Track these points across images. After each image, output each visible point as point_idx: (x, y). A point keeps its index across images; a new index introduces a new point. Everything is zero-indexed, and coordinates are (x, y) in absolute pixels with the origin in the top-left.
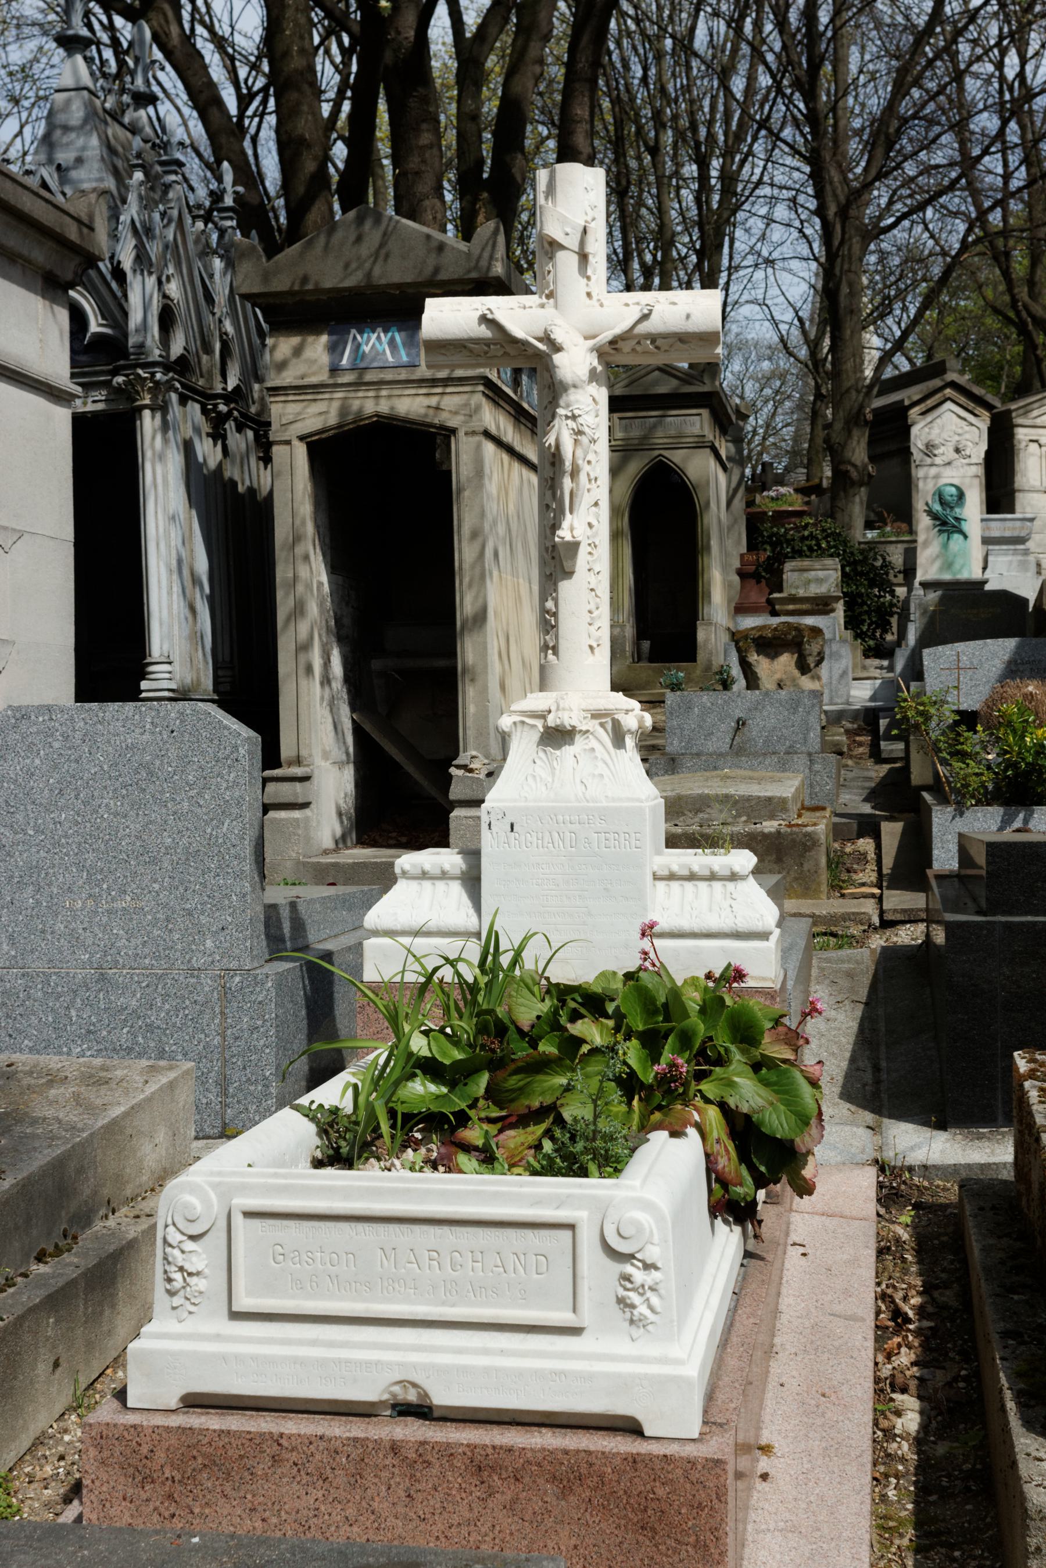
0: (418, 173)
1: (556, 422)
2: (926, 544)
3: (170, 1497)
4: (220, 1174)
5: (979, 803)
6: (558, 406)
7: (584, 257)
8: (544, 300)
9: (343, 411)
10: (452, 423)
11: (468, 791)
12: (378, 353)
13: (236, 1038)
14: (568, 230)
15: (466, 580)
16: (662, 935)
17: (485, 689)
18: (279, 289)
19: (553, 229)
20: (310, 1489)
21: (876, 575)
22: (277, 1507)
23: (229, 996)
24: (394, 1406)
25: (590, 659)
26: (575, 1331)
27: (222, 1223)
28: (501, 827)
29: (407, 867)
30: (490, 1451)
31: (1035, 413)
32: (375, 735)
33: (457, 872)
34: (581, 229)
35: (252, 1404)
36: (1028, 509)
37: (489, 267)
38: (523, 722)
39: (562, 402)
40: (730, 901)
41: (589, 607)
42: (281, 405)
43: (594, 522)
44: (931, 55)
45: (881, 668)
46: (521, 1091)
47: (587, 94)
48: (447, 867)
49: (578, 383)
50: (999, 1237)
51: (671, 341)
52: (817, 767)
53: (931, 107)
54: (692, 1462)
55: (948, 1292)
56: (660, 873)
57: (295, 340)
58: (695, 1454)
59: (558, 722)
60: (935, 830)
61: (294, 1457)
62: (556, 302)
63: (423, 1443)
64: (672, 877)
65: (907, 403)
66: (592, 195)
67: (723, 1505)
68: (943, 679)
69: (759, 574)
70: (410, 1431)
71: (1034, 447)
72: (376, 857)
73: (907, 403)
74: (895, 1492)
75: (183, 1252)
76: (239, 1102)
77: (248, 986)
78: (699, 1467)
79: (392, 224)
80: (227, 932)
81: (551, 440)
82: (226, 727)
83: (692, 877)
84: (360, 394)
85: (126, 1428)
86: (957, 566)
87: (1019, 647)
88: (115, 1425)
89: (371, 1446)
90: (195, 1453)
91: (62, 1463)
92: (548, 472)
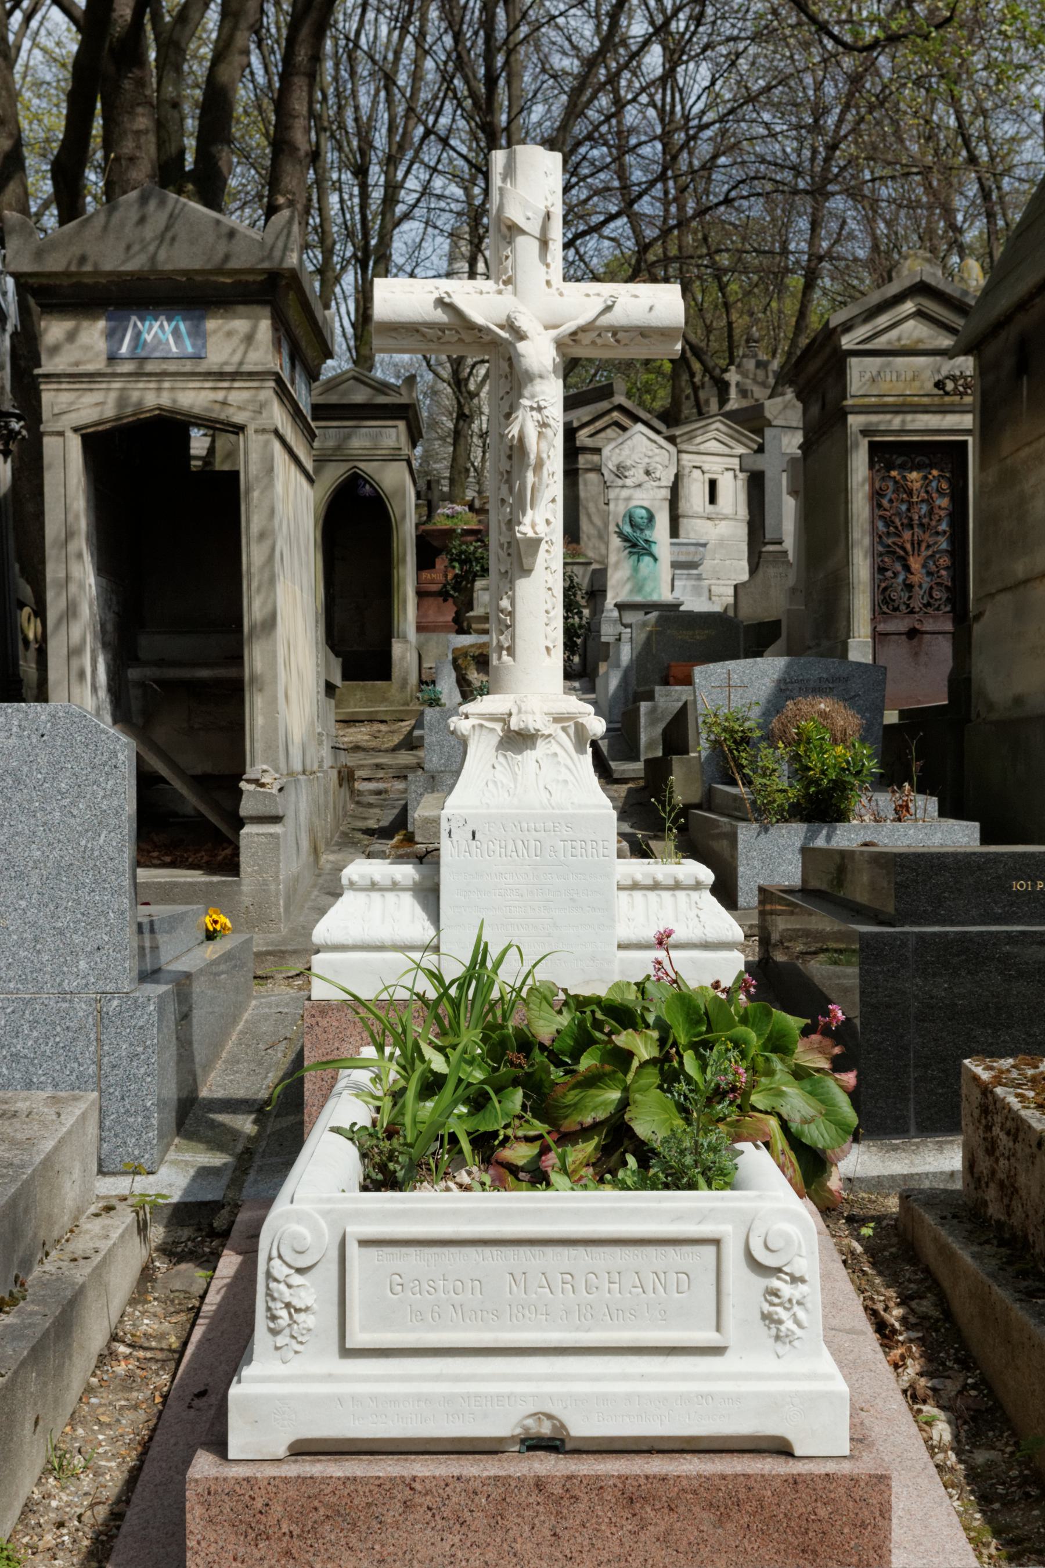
0: (132, 159)
1: (520, 413)
2: (617, 564)
3: (288, 1553)
4: (329, 1200)
6: (520, 396)
7: (544, 243)
8: (502, 286)
10: (239, 418)
12: (160, 342)
13: (114, 1067)
14: (530, 214)
15: (255, 585)
16: (678, 946)
17: (274, 700)
18: (54, 269)
19: (514, 213)
20: (446, 1535)
22: (408, 1557)
23: (106, 1021)
24: (523, 1441)
26: (717, 1351)
27: (334, 1254)
28: (461, 835)
29: (355, 878)
30: (642, 1481)
31: (699, 440)
34: (542, 214)
35: (365, 1448)
36: (692, 535)
38: (481, 726)
39: (526, 393)
41: (546, 607)
42: (53, 393)
43: (552, 519)
44: (602, 79)
46: (575, 1106)
47: (305, 88)
48: (398, 877)
50: (980, 1244)
51: (633, 334)
53: (604, 129)
54: (854, 1480)
55: (925, 1302)
56: (623, 882)
57: (68, 325)
58: (856, 1471)
59: (522, 725)
61: (428, 1500)
62: (515, 288)
63: (570, 1478)
64: (635, 886)
67: (886, 1522)
68: (714, 697)
69: (447, 592)
70: (545, 1465)
71: (697, 473)
74: (958, 1503)
75: (289, 1286)
76: (116, 1135)
77: (127, 1010)
78: (862, 1484)
79: (179, 206)
80: (103, 952)
81: (514, 431)
82: (103, 731)
83: (656, 886)
84: (141, 385)
85: (238, 1482)
86: (648, 589)
87: (789, 666)
88: (225, 1479)
89: (513, 1484)
90: (316, 1503)
91: (65, 1531)
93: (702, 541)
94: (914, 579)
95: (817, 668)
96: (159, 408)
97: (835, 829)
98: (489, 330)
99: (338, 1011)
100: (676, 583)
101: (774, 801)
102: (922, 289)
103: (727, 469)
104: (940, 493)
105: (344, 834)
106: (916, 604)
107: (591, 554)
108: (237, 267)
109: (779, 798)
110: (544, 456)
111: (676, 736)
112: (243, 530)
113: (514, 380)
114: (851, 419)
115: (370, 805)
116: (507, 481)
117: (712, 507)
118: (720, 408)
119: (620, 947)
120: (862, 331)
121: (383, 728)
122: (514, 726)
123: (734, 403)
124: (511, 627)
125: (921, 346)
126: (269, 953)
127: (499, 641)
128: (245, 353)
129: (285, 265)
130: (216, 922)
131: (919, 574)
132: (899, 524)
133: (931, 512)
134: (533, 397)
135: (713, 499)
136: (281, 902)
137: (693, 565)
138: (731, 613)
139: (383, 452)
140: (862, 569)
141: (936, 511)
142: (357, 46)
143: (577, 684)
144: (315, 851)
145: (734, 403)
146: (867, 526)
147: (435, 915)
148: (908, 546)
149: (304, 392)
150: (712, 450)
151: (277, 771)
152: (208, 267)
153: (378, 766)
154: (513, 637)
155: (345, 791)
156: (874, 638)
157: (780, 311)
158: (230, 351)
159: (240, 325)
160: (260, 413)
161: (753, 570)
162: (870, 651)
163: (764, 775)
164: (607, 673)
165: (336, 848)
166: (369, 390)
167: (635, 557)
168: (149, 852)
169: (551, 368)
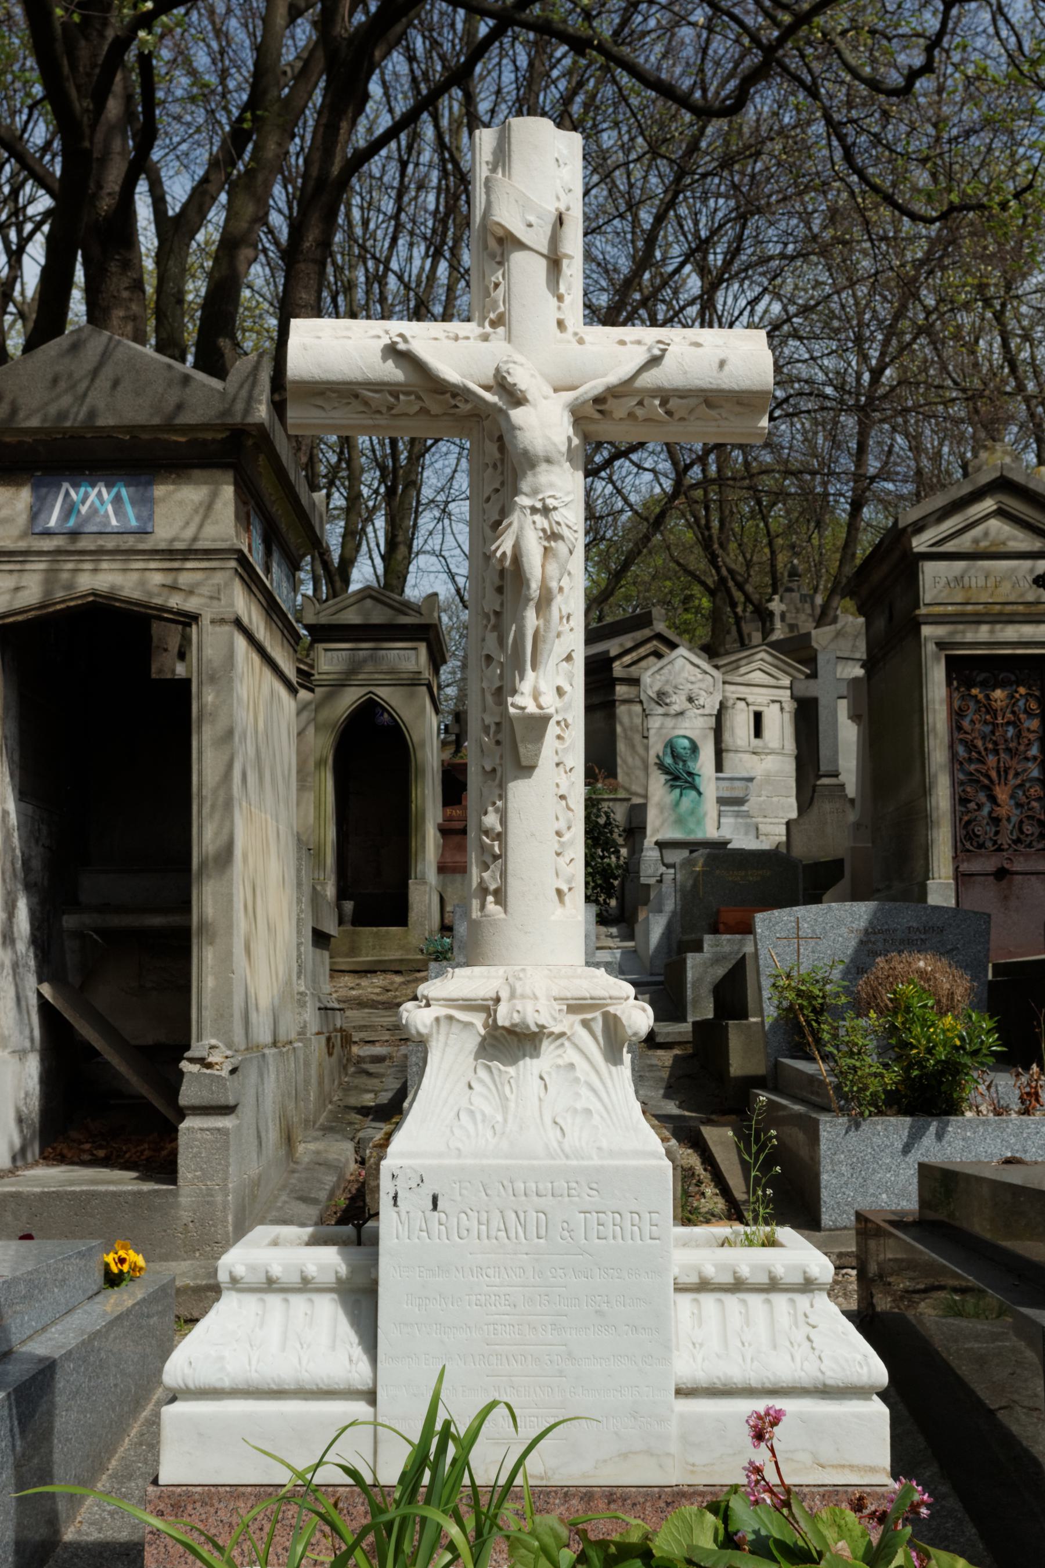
1: (515, 518)
5: (880, 1113)
6: (516, 491)
7: (555, 263)
8: (488, 329)
10: (191, 605)
11: (205, 1093)
14: (532, 219)
15: (206, 810)
17: (227, 957)
19: (508, 216)
21: (600, 833)
25: (558, 913)
28: (414, 1202)
29: (240, 1271)
31: (743, 670)
33: (330, 1279)
34: (552, 218)
37: (248, 410)
38: (450, 1018)
39: (525, 486)
40: (806, 1329)
41: (557, 826)
43: (567, 688)
45: (611, 936)
48: (311, 1270)
49: (554, 455)
51: (692, 402)
56: (684, 1279)
59: (516, 1018)
64: (704, 1286)
65: (613, 653)
68: (779, 950)
72: (72, 1183)
81: (505, 545)
83: (738, 1286)
84: (70, 566)
94: (1002, 812)
95: (907, 917)
96: (94, 593)
98: (467, 390)
99: (204, 1504)
100: (723, 820)
101: (865, 1088)
102: (1003, 485)
103: (773, 701)
104: (1028, 713)
106: (1004, 840)
109: (874, 1086)
110: (554, 585)
111: (732, 993)
114: (926, 631)
116: (496, 628)
117: (757, 741)
118: (764, 639)
119: (680, 1392)
121: (398, 979)
122: (503, 1020)
123: (779, 633)
125: (1002, 549)
127: (482, 878)
128: (201, 526)
129: (250, 420)
130: (122, 1261)
131: (1006, 807)
133: (1019, 735)
134: (535, 492)
135: (758, 733)
136: (230, 1218)
137: (740, 801)
138: (784, 850)
139: (405, 676)
140: (942, 798)
141: (1025, 734)
142: (387, 269)
143: (614, 930)
144: (289, 1140)
147: (370, 1341)
148: (994, 774)
151: (229, 1046)
152: (156, 421)
154: (504, 874)
156: (956, 879)
158: (180, 523)
161: (802, 809)
162: (953, 894)
163: (851, 1054)
164: (647, 919)
165: (320, 1133)
166: (389, 611)
167: (677, 791)
168: (81, 1143)
169: (564, 449)
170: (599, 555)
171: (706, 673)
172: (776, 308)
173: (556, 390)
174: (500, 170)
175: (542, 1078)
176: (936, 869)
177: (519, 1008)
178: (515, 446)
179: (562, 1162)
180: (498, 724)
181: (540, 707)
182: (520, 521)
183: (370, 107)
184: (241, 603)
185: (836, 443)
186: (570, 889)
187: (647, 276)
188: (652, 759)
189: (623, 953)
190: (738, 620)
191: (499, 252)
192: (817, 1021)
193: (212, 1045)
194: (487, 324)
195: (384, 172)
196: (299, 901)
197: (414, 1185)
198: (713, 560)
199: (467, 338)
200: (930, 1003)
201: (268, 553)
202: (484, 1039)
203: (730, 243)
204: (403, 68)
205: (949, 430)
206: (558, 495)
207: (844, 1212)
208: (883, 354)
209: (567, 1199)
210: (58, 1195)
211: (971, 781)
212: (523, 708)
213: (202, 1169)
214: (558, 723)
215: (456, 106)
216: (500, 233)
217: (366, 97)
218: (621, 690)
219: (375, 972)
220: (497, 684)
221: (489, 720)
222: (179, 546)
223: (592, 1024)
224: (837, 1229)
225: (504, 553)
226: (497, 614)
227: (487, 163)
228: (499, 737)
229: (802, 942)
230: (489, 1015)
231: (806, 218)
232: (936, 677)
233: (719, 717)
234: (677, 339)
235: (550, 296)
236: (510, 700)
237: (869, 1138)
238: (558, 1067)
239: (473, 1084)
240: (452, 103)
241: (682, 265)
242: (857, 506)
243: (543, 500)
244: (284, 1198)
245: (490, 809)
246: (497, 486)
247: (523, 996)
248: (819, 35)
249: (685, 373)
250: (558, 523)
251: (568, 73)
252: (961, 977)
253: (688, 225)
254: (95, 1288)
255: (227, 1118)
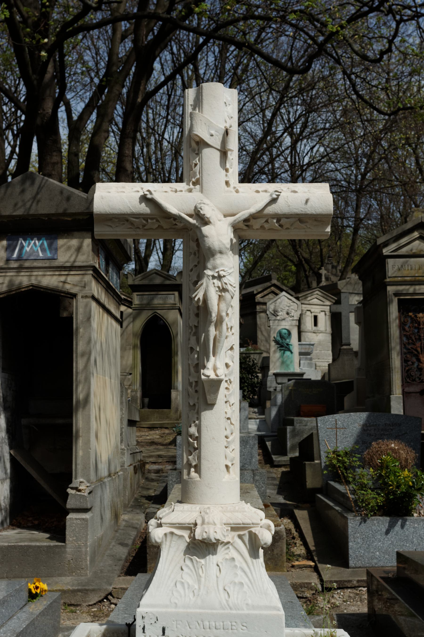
1: (204, 281)
5: (375, 515)
6: (205, 268)
7: (224, 153)
8: (192, 186)
9: (11, 283)
10: (74, 290)
12: (34, 251)
14: (213, 132)
19: (201, 131)
31: (309, 298)
32: (23, 463)
34: (223, 132)
36: (307, 340)
38: (172, 533)
39: (209, 265)
41: (225, 433)
43: (231, 363)
45: (255, 412)
47: (131, 144)
49: (224, 250)
51: (292, 220)
52: (257, 478)
59: (205, 536)
60: (350, 530)
65: (255, 292)
66: (229, 108)
68: (328, 433)
71: (308, 313)
72: (22, 540)
73: (255, 292)
79: (44, 181)
81: (200, 295)
87: (368, 417)
92: (193, 321)
93: (312, 343)
97: (406, 520)
100: (301, 362)
101: (369, 504)
103: (322, 311)
105: (136, 499)
107: (262, 348)
108: (74, 212)
109: (373, 503)
110: (224, 314)
112: (74, 349)
113: (201, 255)
114: (389, 288)
115: (153, 480)
120: (393, 246)
121: (167, 431)
122: (198, 536)
123: (324, 283)
124: (198, 449)
126: (79, 590)
127: (188, 460)
130: (37, 588)
132: (414, 339)
134: (214, 268)
135: (316, 324)
136: (88, 558)
137: (308, 354)
140: (396, 361)
142: (163, 138)
143: (256, 410)
144: (116, 516)
145: (324, 283)
146: (398, 340)
148: (419, 349)
149: (115, 277)
150: (315, 303)
151: (88, 481)
153: (159, 456)
154: (199, 458)
155: (139, 475)
156: (403, 394)
157: (340, 245)
158: (69, 255)
159: (74, 242)
160: (85, 287)
161: (334, 360)
162: (402, 401)
165: (131, 509)
167: (283, 351)
169: (229, 246)
170: (250, 250)
171: (294, 302)
172: (322, 149)
173: (225, 216)
174: (197, 109)
175: (218, 565)
176: (394, 390)
177: (206, 530)
178: (204, 245)
179: (228, 611)
180: (196, 382)
181: (217, 375)
182: (207, 283)
183: (155, 73)
184: (96, 289)
185: (347, 204)
186: (232, 464)
187: (269, 138)
188: (272, 338)
189: (260, 421)
190: (307, 277)
191: (197, 149)
192: (346, 473)
193: (81, 482)
194: (191, 184)
195: (161, 99)
196: (121, 410)
197: (153, 622)
198: (296, 252)
199: (181, 191)
200: (397, 464)
201: (107, 265)
202: (189, 544)
203: (303, 123)
204: (169, 57)
205: (394, 198)
206: (226, 269)
207: (360, 560)
208: (366, 168)
209: (230, 631)
210: (14, 547)
211: (409, 352)
212: (208, 376)
213: (76, 536)
214: (226, 381)
215: (190, 73)
216: (198, 139)
217: (152, 69)
218: (258, 308)
219: (157, 428)
220: (196, 362)
221: (192, 380)
222: (68, 264)
223: (244, 537)
224: (356, 568)
225: (199, 299)
226: (196, 327)
227: (191, 105)
228: (197, 388)
229: (338, 430)
230: (191, 532)
231: (334, 112)
232: (394, 311)
233: (300, 321)
234: (285, 189)
235: (222, 170)
236: (202, 371)
237: (370, 527)
238: (226, 559)
239: (183, 568)
240: (188, 71)
241: (283, 133)
242: (356, 230)
243: (218, 272)
244: (113, 543)
245: (193, 425)
246: (196, 264)
247: (208, 523)
248: (342, 38)
249: (289, 206)
250: (226, 284)
251: (236, 57)
252: (411, 451)
253: (285, 117)
254: (24, 603)
255: (87, 513)
